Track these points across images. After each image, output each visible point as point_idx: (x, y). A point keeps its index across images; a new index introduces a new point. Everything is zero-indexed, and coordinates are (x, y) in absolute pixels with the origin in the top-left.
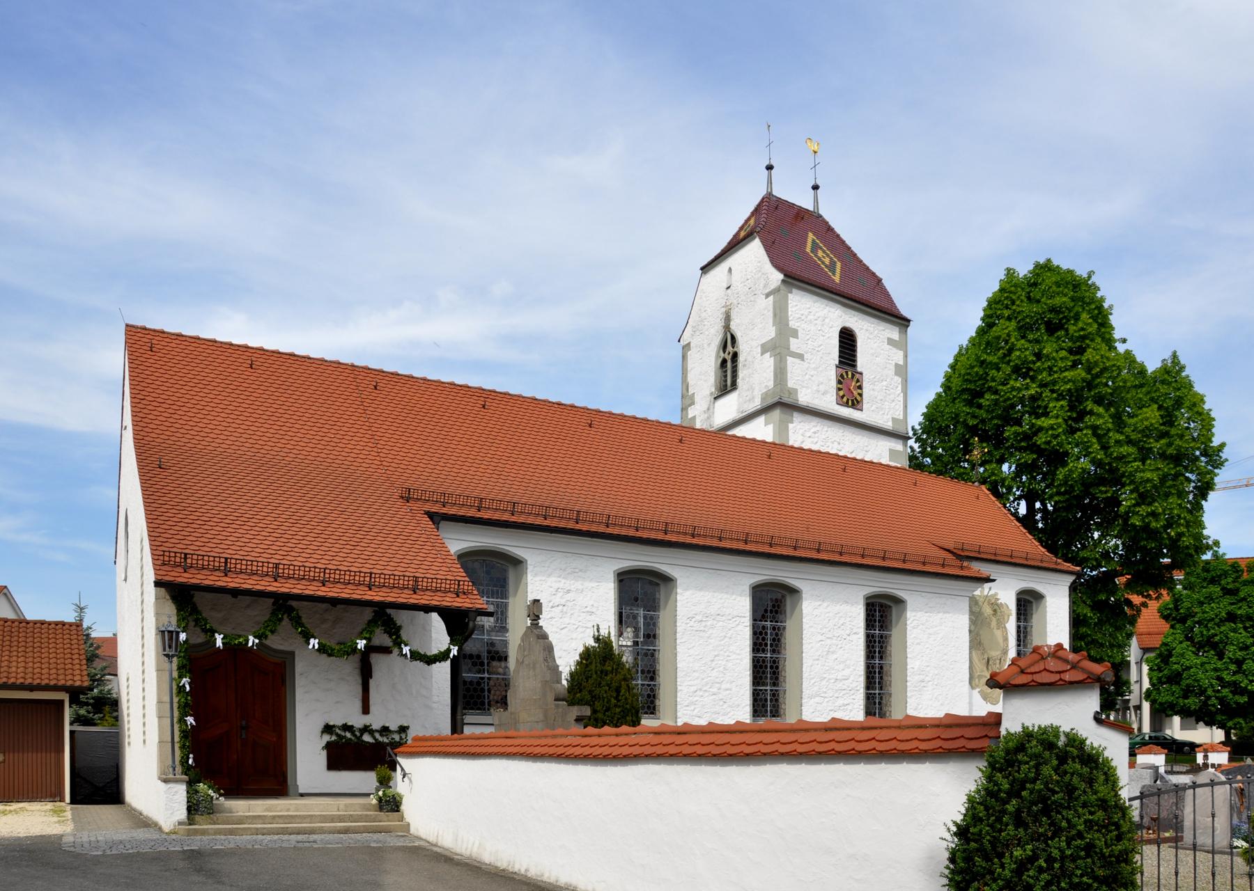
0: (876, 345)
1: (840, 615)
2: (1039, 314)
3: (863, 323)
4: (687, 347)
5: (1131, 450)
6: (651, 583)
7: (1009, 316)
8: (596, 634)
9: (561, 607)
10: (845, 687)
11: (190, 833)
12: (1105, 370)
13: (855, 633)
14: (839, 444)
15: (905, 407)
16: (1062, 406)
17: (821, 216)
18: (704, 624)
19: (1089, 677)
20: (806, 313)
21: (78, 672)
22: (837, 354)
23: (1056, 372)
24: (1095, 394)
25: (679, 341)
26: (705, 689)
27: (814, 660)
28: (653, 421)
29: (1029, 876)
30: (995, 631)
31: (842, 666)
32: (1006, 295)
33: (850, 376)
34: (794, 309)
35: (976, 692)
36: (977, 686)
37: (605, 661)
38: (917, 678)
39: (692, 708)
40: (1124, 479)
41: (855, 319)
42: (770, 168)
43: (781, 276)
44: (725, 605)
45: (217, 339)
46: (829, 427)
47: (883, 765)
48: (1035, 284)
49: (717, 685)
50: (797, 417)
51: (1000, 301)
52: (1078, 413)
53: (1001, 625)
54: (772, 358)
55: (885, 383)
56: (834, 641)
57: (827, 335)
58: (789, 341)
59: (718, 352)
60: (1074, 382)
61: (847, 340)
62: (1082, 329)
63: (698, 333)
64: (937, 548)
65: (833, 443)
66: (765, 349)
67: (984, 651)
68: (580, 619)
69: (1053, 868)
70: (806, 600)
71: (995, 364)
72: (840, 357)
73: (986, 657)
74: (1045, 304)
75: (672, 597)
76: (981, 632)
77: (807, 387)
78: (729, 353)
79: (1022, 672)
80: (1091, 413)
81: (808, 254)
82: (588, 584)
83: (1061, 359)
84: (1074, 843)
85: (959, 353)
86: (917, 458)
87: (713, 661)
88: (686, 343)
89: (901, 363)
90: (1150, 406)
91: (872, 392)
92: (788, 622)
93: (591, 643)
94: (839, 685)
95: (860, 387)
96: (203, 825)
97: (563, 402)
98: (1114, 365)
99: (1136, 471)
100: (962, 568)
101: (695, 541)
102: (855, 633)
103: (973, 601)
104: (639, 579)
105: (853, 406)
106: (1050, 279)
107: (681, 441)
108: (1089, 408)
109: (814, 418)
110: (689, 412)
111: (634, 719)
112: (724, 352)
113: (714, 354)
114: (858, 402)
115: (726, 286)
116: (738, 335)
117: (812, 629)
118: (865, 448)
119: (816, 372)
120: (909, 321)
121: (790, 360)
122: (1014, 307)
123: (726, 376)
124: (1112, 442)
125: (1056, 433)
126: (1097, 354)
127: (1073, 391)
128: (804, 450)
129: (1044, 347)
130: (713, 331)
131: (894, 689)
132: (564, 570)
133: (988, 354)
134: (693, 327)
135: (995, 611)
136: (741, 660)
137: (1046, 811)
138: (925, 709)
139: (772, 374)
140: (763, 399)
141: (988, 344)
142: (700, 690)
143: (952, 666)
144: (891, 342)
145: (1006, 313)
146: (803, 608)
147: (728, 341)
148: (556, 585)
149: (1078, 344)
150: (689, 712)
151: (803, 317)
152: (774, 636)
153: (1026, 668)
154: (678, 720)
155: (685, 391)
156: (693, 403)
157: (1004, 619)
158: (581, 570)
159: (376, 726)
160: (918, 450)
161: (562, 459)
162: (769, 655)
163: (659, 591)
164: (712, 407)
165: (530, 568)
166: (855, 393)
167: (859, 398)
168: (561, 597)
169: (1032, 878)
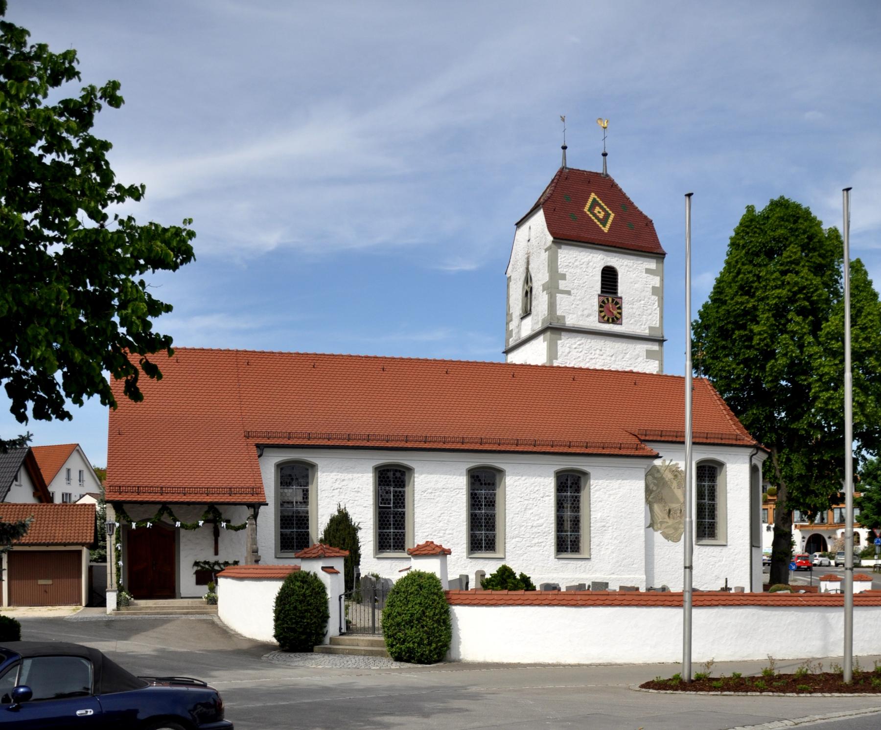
3: (623, 261)
9: (338, 490)
10: (539, 531)
11: (116, 614)
14: (601, 350)
15: (662, 317)
18: (433, 494)
21: (89, 534)
23: (769, 290)
27: (516, 514)
28: (431, 360)
31: (536, 518)
34: (563, 260)
36: (660, 529)
41: (616, 259)
42: (564, 148)
44: (449, 482)
46: (592, 339)
48: (768, 218)
50: (564, 336)
55: (642, 302)
56: (531, 502)
57: (591, 274)
59: (524, 286)
61: (609, 277)
65: (595, 350)
68: (350, 496)
70: (508, 476)
72: (602, 288)
73: (667, 508)
74: (769, 235)
77: (574, 313)
82: (356, 475)
87: (440, 517)
89: (658, 285)
91: (630, 310)
93: (337, 513)
94: (535, 530)
95: (620, 308)
96: (124, 610)
97: (369, 355)
105: (613, 322)
110: (510, 326)
114: (618, 319)
116: (533, 275)
117: (513, 495)
118: (624, 352)
119: (581, 302)
121: (559, 296)
125: (762, 337)
132: (341, 468)
135: (676, 476)
136: (460, 515)
138: (607, 545)
140: (543, 323)
142: (431, 534)
143: (629, 516)
144: (648, 271)
147: (528, 279)
148: (336, 477)
151: (570, 265)
156: (511, 320)
158: (351, 468)
159: (221, 561)
165: (319, 469)
166: (615, 312)
167: (618, 316)
168: (339, 484)
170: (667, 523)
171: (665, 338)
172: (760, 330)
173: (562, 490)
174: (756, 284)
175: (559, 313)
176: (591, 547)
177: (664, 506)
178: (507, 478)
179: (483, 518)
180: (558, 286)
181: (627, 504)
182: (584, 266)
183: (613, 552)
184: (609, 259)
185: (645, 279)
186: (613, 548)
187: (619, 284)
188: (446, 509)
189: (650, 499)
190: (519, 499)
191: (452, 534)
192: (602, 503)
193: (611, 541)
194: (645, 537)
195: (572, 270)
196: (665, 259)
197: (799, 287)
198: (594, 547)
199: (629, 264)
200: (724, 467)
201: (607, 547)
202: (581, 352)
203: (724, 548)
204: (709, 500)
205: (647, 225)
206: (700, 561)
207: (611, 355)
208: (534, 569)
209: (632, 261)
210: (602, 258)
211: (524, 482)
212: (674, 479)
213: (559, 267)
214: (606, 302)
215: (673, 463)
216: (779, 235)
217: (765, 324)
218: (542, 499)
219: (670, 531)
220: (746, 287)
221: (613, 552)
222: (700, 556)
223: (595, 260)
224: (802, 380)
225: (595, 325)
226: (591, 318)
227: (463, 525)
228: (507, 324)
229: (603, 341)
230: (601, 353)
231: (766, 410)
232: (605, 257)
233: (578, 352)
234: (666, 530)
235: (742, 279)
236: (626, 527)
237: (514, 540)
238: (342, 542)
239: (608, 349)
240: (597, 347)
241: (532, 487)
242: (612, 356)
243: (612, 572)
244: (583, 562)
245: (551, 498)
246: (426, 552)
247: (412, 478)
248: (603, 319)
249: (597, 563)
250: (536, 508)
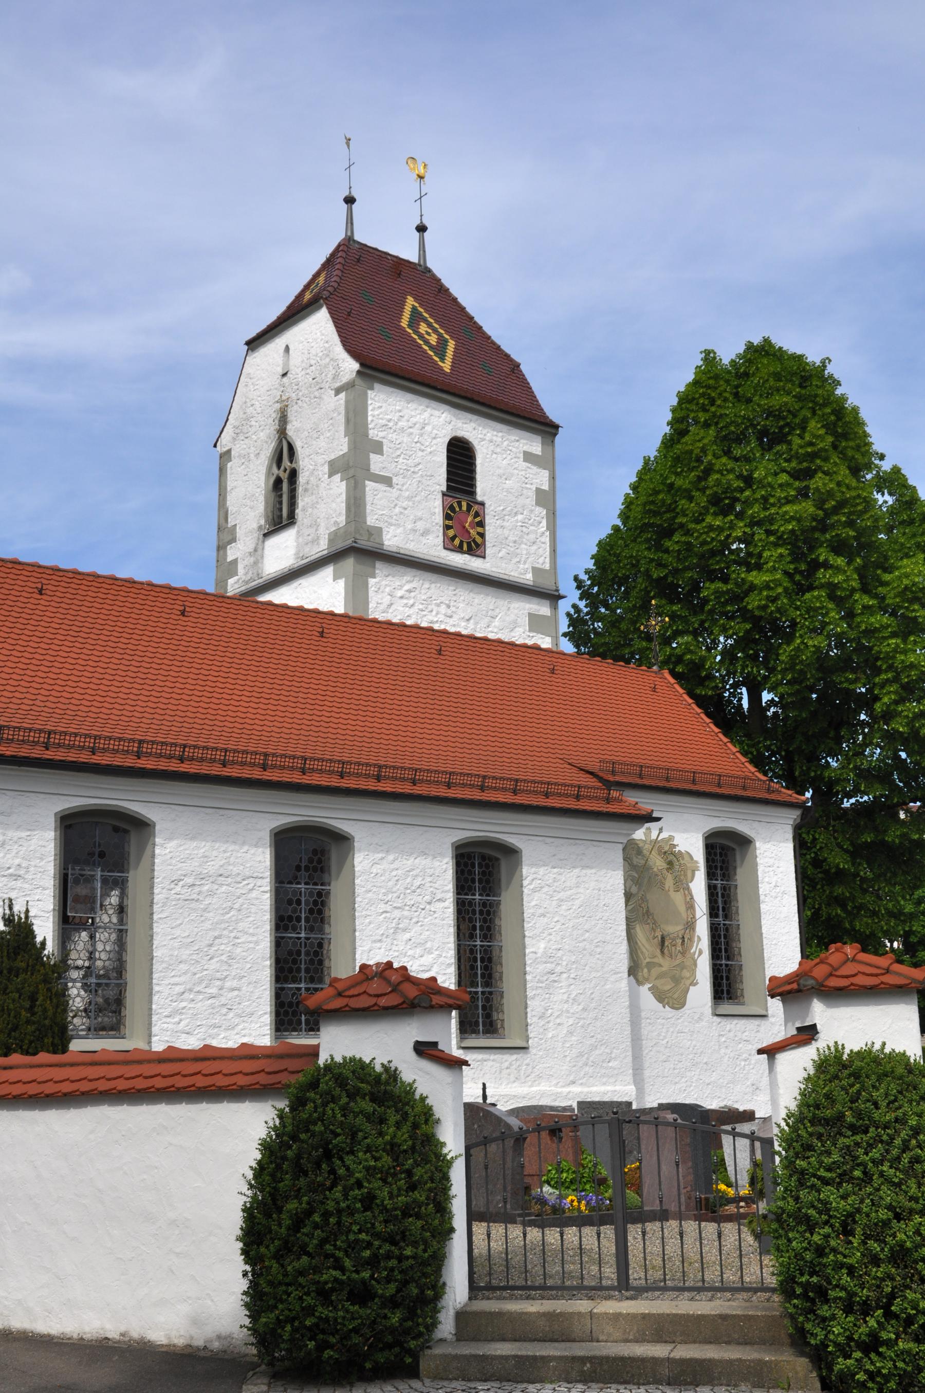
0: (504, 462)
1: (414, 873)
2: (749, 420)
3: (485, 431)
4: (226, 456)
5: (886, 619)
6: (116, 829)
7: (706, 421)
8: (7, 912)
12: (842, 504)
13: (439, 900)
14: (448, 606)
15: (554, 551)
16: (781, 555)
17: (430, 271)
18: (197, 889)
19: (404, 1002)
20: (396, 419)
22: (444, 475)
23: (773, 505)
24: (833, 537)
25: (215, 446)
26: (197, 989)
27: (375, 941)
29: (303, 1234)
30: (672, 894)
31: (418, 951)
32: (701, 391)
33: (464, 508)
34: (376, 413)
35: (645, 991)
36: (647, 980)
37: (16, 954)
38: (541, 967)
39: (176, 1020)
40: (879, 663)
41: (473, 425)
42: (350, 200)
43: (356, 366)
44: (232, 860)
47: (204, 1105)
48: (746, 375)
49: (218, 983)
50: (381, 568)
51: (694, 399)
52: (809, 564)
53: (682, 885)
54: (344, 483)
55: (520, 517)
56: (406, 913)
57: (429, 450)
58: (369, 459)
59: (269, 468)
60: (799, 520)
62: (811, 444)
63: (241, 437)
64: (574, 770)
65: (438, 605)
66: (335, 467)
67: (655, 925)
69: (328, 1224)
70: (360, 851)
71: (686, 490)
72: (448, 480)
74: (759, 405)
75: (148, 852)
76: (648, 896)
77: (398, 526)
78: (285, 470)
79: (340, 994)
80: (826, 565)
81: (403, 329)
82: (13, 834)
83: (781, 485)
84: (351, 1193)
85: (644, 468)
86: (585, 622)
87: (211, 945)
88: (225, 450)
89: (546, 487)
90: (914, 555)
91: (499, 531)
92: (333, 883)
95: (481, 524)
98: (859, 496)
99: (895, 651)
100: (608, 800)
101: (184, 768)
102: (439, 900)
103: (632, 852)
104: (97, 823)
106: (767, 367)
107: (183, 613)
108: (822, 558)
109: (409, 570)
110: (229, 552)
111: (57, 1041)
112: (279, 467)
113: (263, 470)
114: (478, 545)
115: (281, 372)
116: (298, 445)
117: (370, 895)
118: (490, 613)
119: (410, 504)
120: (556, 427)
121: (370, 485)
122: (713, 409)
123: (281, 503)
124: (858, 608)
125: (773, 594)
126: (831, 480)
127: (798, 533)
128: (379, 622)
129: (756, 468)
130: (262, 435)
131: (508, 985)
133: (677, 474)
134: (236, 427)
135: (670, 864)
136: (257, 943)
137: (328, 1155)
138: (558, 1017)
139: (344, 505)
140: (331, 541)
141: (677, 460)
142: (191, 990)
143: (599, 950)
144: (529, 457)
145: (702, 417)
146: (356, 863)
149: (805, 464)
150: (170, 1026)
151: (391, 424)
152: (311, 906)
153: (345, 991)
154: (154, 1039)
155: (222, 521)
156: (233, 540)
157: (685, 875)
160: (585, 610)
161: (22, 627)
162: (303, 935)
163: (129, 842)
164: (260, 547)
167: (479, 539)
169: (307, 1235)
170: (661, 966)
171: (562, 592)
172: (767, 579)
174: (747, 493)
175: (371, 521)
176: (529, 1021)
177: (654, 930)
178: (356, 856)
179: (303, 950)
180: (369, 465)
181: (593, 923)
182: (415, 431)
183: (571, 1033)
184: (459, 424)
185: (523, 473)
186: (571, 1021)
187: (478, 477)
188: (223, 926)
190: (382, 907)
191: (239, 989)
192: (546, 920)
193: (566, 1006)
194: (630, 996)
195: (394, 436)
196: (557, 438)
197: (837, 501)
198: (535, 1019)
199: (495, 438)
200: (752, 846)
201: (558, 1021)
202: (412, 605)
203: (762, 1022)
205: (513, 371)
206: (723, 1051)
207: (467, 617)
209: (500, 434)
210: (448, 419)
211: (392, 866)
212: (668, 869)
213: (370, 426)
214: (457, 509)
215: (664, 835)
216: (781, 406)
217: (774, 569)
218: (428, 907)
219: (666, 985)
220: (727, 498)
221: (571, 1033)
222: (723, 1039)
223: (434, 421)
224: (847, 680)
225: (436, 554)
226: (431, 537)
227: (264, 966)
228: (221, 548)
229: (452, 588)
230: (449, 612)
231: (759, 742)
232: (454, 419)
233: (406, 605)
234: (659, 983)
235: (718, 483)
236: (593, 974)
238: (27, 1004)
239: (461, 605)
240: (443, 599)
241: (409, 880)
242: (468, 620)
243: (571, 1078)
244: (515, 1057)
245: (447, 904)
246: (364, 1002)
247: (149, 847)
248: (451, 544)
249: (541, 1057)
250: (417, 928)
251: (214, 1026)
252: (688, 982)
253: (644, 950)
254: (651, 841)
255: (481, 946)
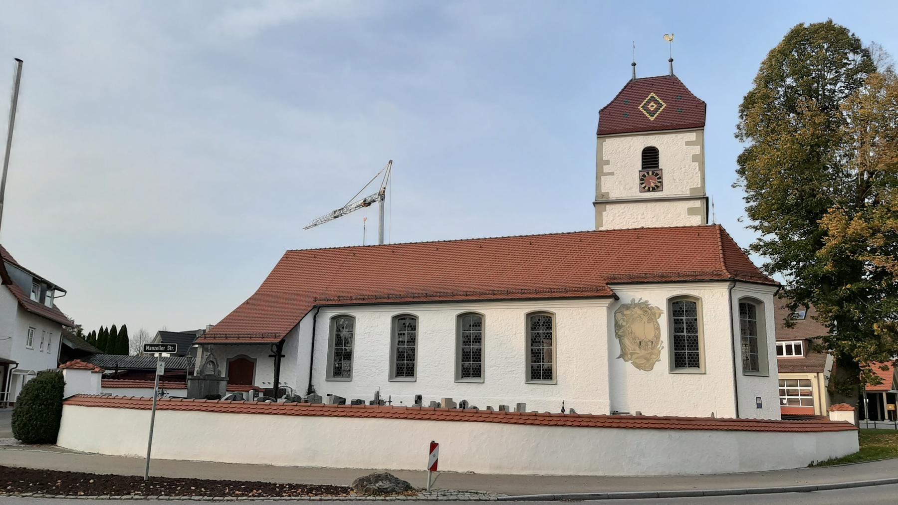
10: (512, 361)
26: (431, 364)
36: (630, 359)
45: (492, 237)
61: (650, 157)
87: (436, 351)
89: (698, 153)
105: (654, 190)
142: (429, 364)
143: (592, 348)
144: (688, 143)
167: (659, 184)
170: (638, 354)
173: (535, 328)
189: (619, 333)
191: (444, 364)
201: (571, 375)
204: (750, 334)
208: (508, 392)
234: (635, 360)
237: (492, 368)
245: (522, 334)
248: (643, 190)
251: (436, 375)
252: (655, 360)
253: (629, 348)
254: (635, 304)
255: (688, 353)
